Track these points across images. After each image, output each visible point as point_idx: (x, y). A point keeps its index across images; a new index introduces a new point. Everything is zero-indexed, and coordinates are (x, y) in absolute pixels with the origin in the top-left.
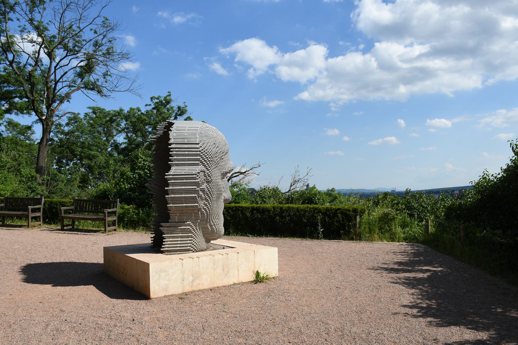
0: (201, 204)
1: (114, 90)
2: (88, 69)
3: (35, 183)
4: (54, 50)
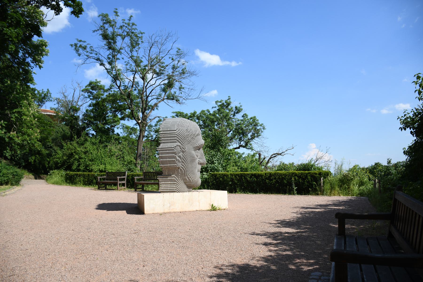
0: (180, 165)
2: (170, 85)
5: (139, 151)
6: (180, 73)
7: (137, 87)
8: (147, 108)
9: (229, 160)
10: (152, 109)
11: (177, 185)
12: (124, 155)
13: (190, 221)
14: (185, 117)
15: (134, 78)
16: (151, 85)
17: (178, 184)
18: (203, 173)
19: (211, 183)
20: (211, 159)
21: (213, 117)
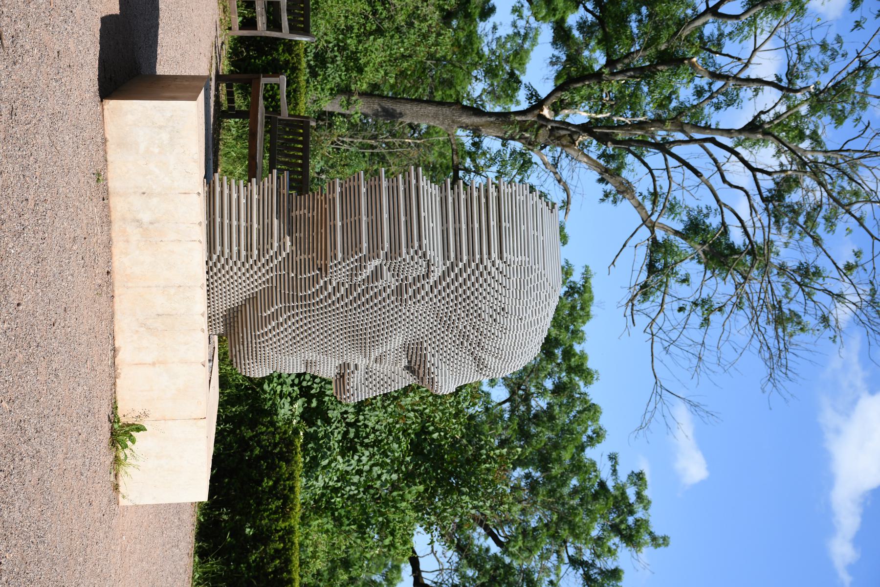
0: (339, 274)
3: (340, 76)
4: (772, 138)
5: (409, 106)
6: (780, 302)
7: (711, 97)
9: (362, 532)
10: (607, 170)
11: (243, 259)
12: (392, 37)
13: (61, 311)
16: (723, 168)
17: (247, 266)
18: (299, 402)
20: (366, 441)
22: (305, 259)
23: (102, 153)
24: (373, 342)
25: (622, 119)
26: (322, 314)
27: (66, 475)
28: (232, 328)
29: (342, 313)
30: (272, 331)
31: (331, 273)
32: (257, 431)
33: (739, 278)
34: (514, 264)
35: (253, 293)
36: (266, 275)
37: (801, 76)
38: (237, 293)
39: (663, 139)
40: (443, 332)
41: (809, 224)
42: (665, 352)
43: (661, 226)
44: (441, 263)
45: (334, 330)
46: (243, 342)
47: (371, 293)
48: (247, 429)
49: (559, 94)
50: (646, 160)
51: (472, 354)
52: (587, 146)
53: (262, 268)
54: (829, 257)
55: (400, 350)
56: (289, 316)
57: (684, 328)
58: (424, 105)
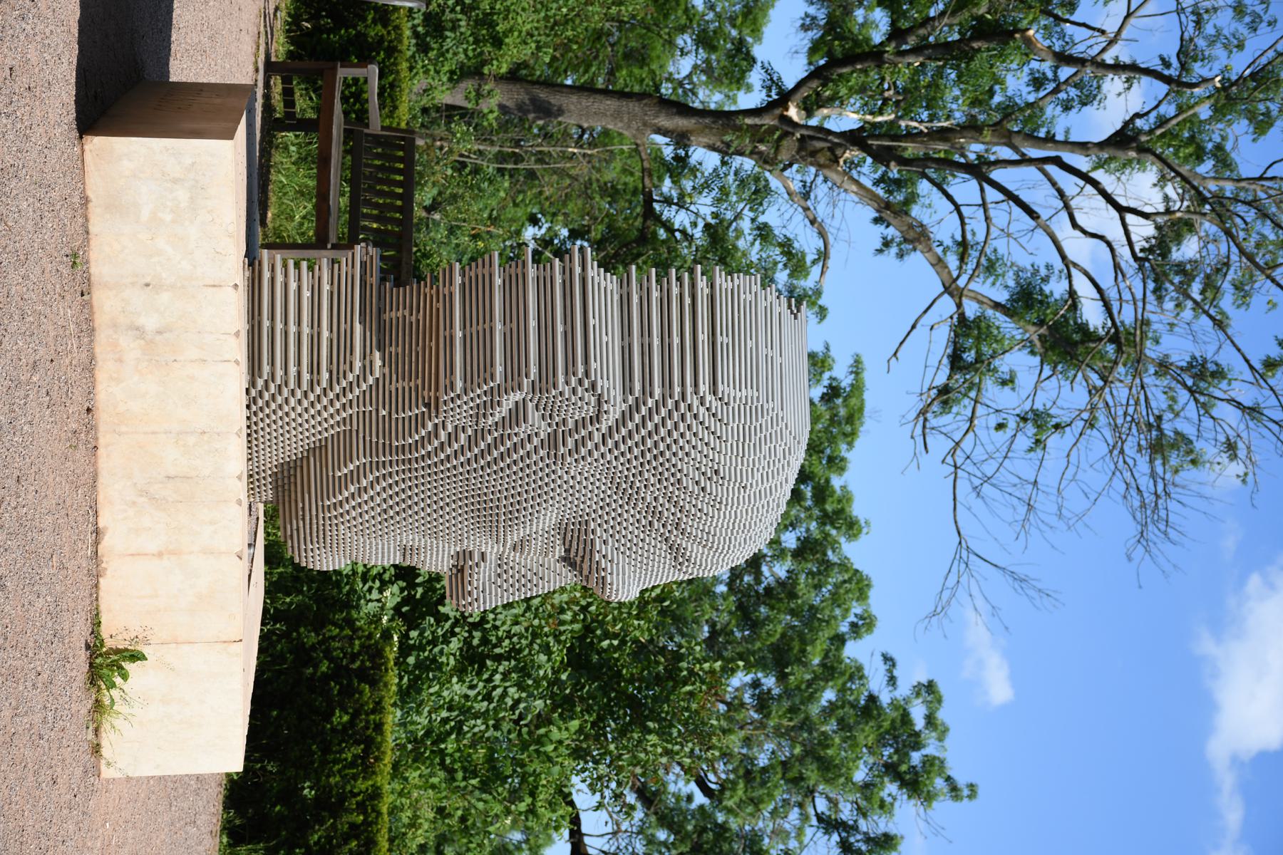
0: (458, 414)
1: (960, 472)
3: (465, 51)
4: (1151, 158)
5: (574, 98)
6: (1159, 418)
7: (1056, 91)
8: (894, 172)
11: (305, 386)
14: (813, 448)
15: (1132, 70)
16: (1073, 203)
17: (312, 397)
19: (311, 638)
20: (498, 651)
21: (816, 661)
22: (404, 388)
23: (81, 220)
24: (510, 519)
25: (914, 124)
26: (429, 475)
27: (16, 742)
28: (286, 493)
29: (461, 474)
30: (350, 500)
31: (445, 411)
32: (324, 635)
33: (1096, 380)
34: (735, 402)
35: (320, 440)
36: (342, 411)
37: (1200, 56)
38: (294, 439)
39: (979, 157)
40: (620, 506)
41: (1209, 294)
42: (974, 495)
43: (972, 295)
44: (619, 399)
45: (448, 500)
46: (303, 515)
47: (509, 444)
48: (309, 632)
49: (814, 84)
50: (950, 190)
51: (666, 540)
52: (857, 165)
53: (335, 401)
54: (1239, 350)
55: (552, 533)
56: (378, 478)
57: (1005, 457)
58: (598, 97)
